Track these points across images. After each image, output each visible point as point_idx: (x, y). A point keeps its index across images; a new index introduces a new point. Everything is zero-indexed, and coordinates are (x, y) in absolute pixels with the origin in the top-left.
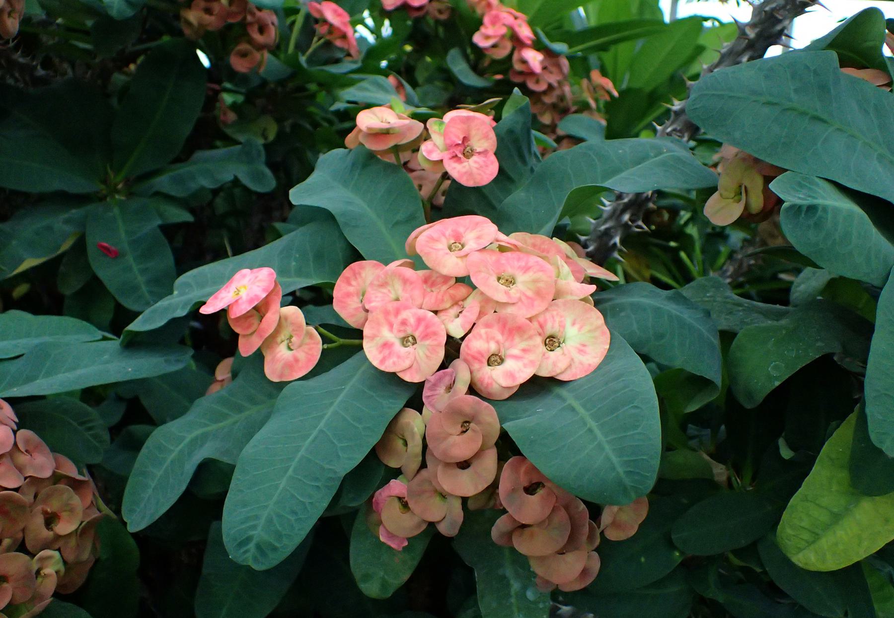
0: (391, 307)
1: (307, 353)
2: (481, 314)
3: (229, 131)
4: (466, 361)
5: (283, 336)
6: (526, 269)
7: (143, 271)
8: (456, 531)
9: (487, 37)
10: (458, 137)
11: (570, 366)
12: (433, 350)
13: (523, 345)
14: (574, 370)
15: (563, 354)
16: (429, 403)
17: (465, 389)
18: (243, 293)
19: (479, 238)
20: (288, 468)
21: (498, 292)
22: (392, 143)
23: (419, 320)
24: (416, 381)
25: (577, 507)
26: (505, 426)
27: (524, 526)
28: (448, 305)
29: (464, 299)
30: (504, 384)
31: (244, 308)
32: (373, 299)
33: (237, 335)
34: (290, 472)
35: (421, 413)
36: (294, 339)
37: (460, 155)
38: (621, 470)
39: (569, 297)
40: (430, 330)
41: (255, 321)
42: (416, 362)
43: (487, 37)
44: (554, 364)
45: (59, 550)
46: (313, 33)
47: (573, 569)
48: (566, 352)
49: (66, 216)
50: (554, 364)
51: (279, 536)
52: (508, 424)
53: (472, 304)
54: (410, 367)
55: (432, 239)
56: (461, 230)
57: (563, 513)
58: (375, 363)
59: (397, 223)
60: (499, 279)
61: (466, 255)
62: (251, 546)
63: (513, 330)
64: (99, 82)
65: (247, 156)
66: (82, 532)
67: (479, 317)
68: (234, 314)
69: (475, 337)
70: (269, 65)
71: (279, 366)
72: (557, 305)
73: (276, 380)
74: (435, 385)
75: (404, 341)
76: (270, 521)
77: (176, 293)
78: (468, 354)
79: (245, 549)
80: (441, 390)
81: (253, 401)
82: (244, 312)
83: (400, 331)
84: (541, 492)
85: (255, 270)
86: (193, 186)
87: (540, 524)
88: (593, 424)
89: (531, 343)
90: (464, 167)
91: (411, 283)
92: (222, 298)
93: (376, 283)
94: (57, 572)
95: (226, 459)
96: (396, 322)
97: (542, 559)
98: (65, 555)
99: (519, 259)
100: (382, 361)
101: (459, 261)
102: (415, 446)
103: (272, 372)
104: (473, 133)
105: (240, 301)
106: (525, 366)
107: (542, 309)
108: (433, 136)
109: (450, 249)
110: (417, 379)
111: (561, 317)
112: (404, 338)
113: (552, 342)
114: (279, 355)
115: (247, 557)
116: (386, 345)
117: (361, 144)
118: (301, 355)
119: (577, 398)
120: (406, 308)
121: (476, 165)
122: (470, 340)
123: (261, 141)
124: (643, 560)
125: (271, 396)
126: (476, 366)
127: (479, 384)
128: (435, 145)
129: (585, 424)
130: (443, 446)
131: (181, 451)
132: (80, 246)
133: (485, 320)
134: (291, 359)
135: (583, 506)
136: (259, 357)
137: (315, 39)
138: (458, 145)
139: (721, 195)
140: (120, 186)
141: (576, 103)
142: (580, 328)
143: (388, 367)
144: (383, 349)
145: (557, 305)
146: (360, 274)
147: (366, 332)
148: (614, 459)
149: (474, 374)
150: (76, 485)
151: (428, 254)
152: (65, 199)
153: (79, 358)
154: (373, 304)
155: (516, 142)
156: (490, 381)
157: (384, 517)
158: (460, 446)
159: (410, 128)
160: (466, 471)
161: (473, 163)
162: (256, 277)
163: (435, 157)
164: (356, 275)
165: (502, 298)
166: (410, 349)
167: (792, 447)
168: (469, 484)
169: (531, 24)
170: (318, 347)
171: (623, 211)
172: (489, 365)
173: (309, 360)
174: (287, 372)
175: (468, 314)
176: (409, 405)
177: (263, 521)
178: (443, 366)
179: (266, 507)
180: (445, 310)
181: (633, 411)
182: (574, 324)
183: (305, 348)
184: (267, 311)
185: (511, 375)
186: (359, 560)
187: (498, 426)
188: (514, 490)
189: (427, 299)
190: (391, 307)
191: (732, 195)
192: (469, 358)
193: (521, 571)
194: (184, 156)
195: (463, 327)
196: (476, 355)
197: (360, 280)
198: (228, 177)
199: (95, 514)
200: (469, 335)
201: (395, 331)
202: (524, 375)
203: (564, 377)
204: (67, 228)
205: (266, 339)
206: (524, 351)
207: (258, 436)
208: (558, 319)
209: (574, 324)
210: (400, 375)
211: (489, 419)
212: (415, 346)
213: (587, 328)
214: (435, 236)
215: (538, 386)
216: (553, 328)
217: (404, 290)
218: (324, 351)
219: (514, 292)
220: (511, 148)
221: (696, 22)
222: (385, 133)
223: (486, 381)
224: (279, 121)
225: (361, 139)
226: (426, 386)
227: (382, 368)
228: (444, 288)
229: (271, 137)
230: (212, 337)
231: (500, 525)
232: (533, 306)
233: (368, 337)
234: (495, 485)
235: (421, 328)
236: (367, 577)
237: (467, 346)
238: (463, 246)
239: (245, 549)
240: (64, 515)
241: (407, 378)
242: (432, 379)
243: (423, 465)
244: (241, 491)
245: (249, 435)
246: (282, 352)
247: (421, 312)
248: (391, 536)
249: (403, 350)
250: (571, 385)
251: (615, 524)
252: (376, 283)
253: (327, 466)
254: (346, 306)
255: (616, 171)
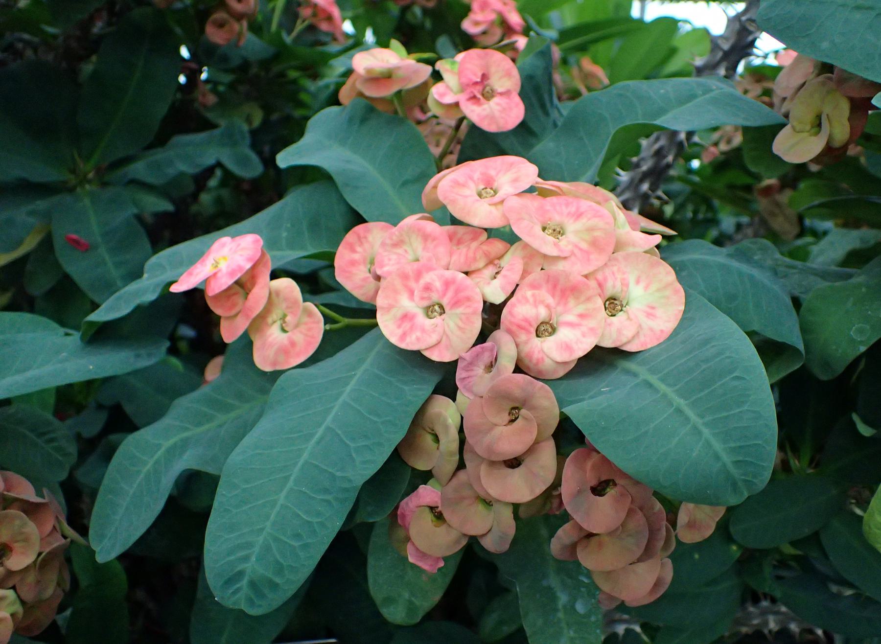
0: (409, 269)
1: (306, 335)
2: (525, 273)
3: (211, 116)
4: (509, 331)
5: (275, 315)
6: (578, 215)
7: (118, 265)
8: (507, 546)
9: (477, 23)
10: (475, 75)
11: (637, 334)
12: (468, 319)
13: (581, 309)
14: (642, 338)
15: (629, 319)
16: (464, 387)
17: (513, 367)
18: (223, 265)
19: (516, 180)
20: (287, 478)
21: (546, 244)
22: (395, 89)
23: (447, 284)
24: (447, 359)
25: (652, 508)
26: (567, 410)
27: (590, 535)
28: (481, 264)
29: (500, 257)
30: (559, 359)
31: (225, 282)
32: (386, 261)
33: (219, 317)
34: (290, 484)
35: (454, 400)
36: (288, 319)
37: (479, 96)
38: (727, 459)
39: (631, 250)
40: (462, 295)
41: (239, 300)
42: (446, 336)
43: (477, 23)
44: (619, 331)
45: (14, 588)
46: (296, 16)
47: (642, 581)
48: (632, 317)
49: (30, 207)
50: (619, 331)
51: (280, 569)
52: (569, 408)
53: (513, 261)
54: (439, 343)
55: (457, 184)
56: (492, 173)
57: (640, 515)
58: (394, 340)
59: (405, 183)
60: (544, 229)
61: (502, 202)
62: (245, 582)
63: (565, 291)
64: (64, 65)
65: (230, 139)
66: (43, 564)
67: (523, 277)
68: (212, 291)
69: (519, 301)
70: (252, 45)
71: (271, 353)
72: (616, 259)
73: (268, 369)
74: (471, 364)
75: (429, 311)
76: (267, 548)
77: (145, 276)
78: (511, 323)
79: (235, 587)
80: (480, 370)
81: (241, 397)
82: (224, 287)
83: (422, 298)
84: (611, 492)
85: (238, 238)
86: (171, 172)
87: (611, 534)
88: (681, 402)
89: (590, 306)
90: (484, 110)
91: (434, 239)
92: (197, 274)
93: (388, 242)
94: (12, 615)
95: (210, 469)
96: (417, 287)
97: (608, 574)
98: (22, 595)
99: (567, 205)
100: (403, 337)
101: (493, 208)
102: (450, 442)
103: (263, 360)
104: (493, 70)
105: (219, 275)
106: (584, 335)
107: (600, 263)
108: (445, 75)
109: (480, 195)
110: (447, 358)
111: (624, 273)
112: (430, 307)
113: (613, 304)
114: (270, 339)
115: (235, 598)
116: (406, 317)
117: (361, 95)
118: (298, 337)
119: (653, 371)
120: (430, 269)
121: (498, 108)
122: (514, 305)
123: (245, 128)
124: (697, 556)
125: (265, 391)
126: (523, 337)
127: (526, 361)
128: (448, 87)
129: (670, 404)
130: (488, 439)
131: (157, 462)
132: (47, 244)
133: (520, 287)
134: (286, 342)
135: (658, 506)
136: (246, 343)
137: (299, 22)
138: (476, 83)
139: (793, 128)
140: (91, 175)
141: (566, 91)
142: (646, 288)
143: (410, 344)
144: (402, 322)
145: (616, 259)
146: (365, 237)
147: (380, 302)
148: (718, 446)
149: (521, 347)
150: (31, 509)
151: (454, 202)
152: (29, 189)
153: (39, 358)
154: (386, 269)
155: (537, 90)
156: (540, 356)
157: (413, 532)
158: (509, 439)
159: (416, 72)
160: (517, 470)
161: (494, 106)
162: (239, 245)
163: (449, 99)
164: (360, 239)
165: (554, 252)
166: (438, 320)
167: (867, 422)
168: (521, 487)
169: (521, 11)
170: (319, 328)
171: (641, 181)
172: (538, 336)
173: (309, 344)
174: (281, 358)
175: (508, 273)
176: (438, 390)
177: (256, 549)
178: (482, 338)
179: (262, 529)
180: (478, 270)
181: (736, 383)
182: (638, 282)
183: (303, 328)
184: (253, 284)
185: (568, 347)
186: (379, 580)
187: (558, 412)
188: (579, 492)
189: (455, 258)
190: (409, 269)
191: (808, 127)
192: (514, 328)
193: (569, 581)
194: (161, 140)
195: (503, 288)
196: (523, 324)
197: (366, 246)
198: (210, 161)
199: (58, 542)
200: (513, 300)
201: (416, 298)
202: (584, 347)
203: (631, 348)
204: (31, 220)
205: (254, 320)
206: (582, 316)
207: (247, 441)
208: (619, 276)
209: (638, 282)
210: (426, 353)
211: (545, 403)
212: (444, 316)
213: (654, 287)
214: (461, 180)
215: (601, 360)
216: (614, 286)
217: (424, 249)
218: (326, 333)
219: (565, 244)
220: (535, 91)
221: (669, 24)
222: (387, 76)
223: (536, 356)
224: (268, 109)
225: (360, 86)
226: (460, 365)
227: (403, 346)
228: (474, 245)
229: (257, 121)
230: (192, 327)
231: (564, 535)
232: (589, 260)
233: (382, 308)
234: (557, 484)
235: (450, 294)
236: (390, 600)
237: (510, 313)
238: (496, 192)
239: (235, 587)
240: (16, 546)
241: (435, 356)
242: (468, 356)
243: (461, 466)
244: (226, 510)
245: (237, 438)
246: (274, 335)
247: (448, 274)
248: (423, 555)
249: (428, 322)
250: (640, 357)
251: (692, 525)
252: (388, 242)
253: (338, 474)
254: (351, 274)
255: (662, 112)
